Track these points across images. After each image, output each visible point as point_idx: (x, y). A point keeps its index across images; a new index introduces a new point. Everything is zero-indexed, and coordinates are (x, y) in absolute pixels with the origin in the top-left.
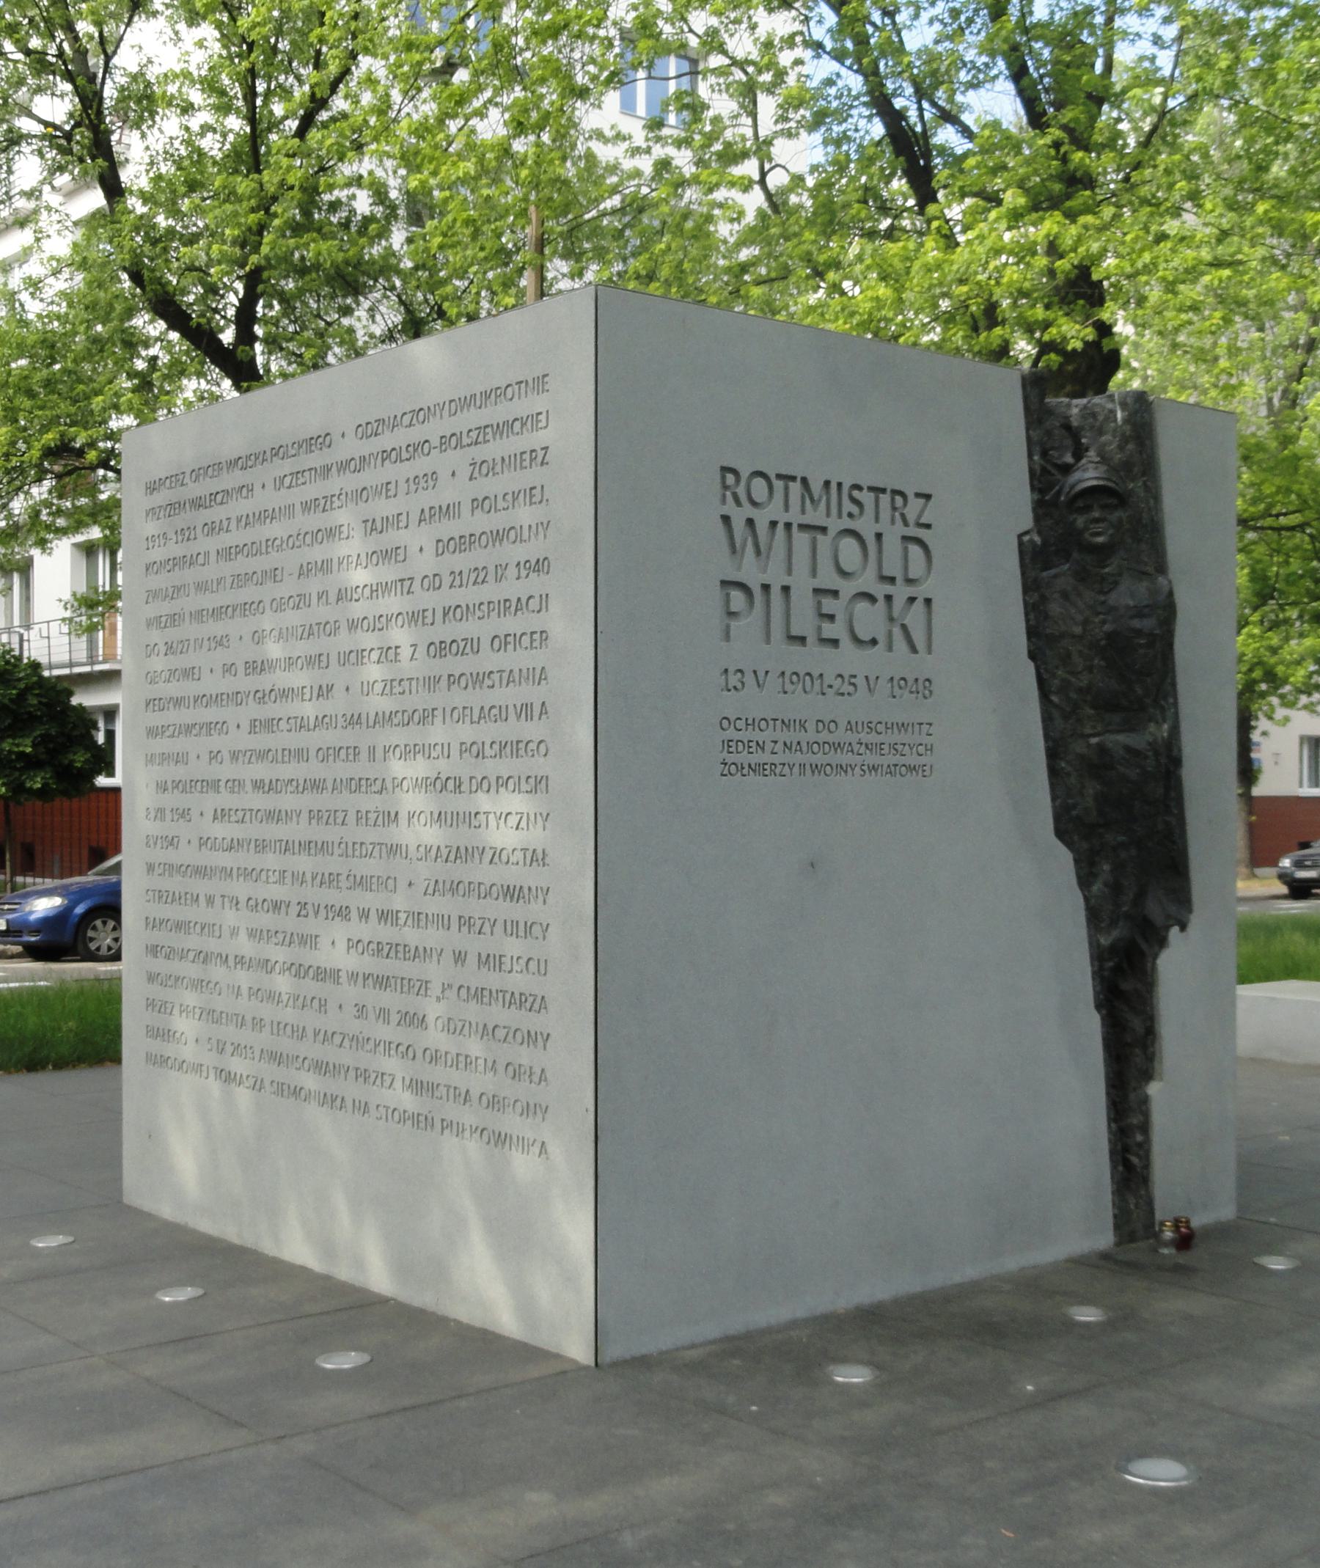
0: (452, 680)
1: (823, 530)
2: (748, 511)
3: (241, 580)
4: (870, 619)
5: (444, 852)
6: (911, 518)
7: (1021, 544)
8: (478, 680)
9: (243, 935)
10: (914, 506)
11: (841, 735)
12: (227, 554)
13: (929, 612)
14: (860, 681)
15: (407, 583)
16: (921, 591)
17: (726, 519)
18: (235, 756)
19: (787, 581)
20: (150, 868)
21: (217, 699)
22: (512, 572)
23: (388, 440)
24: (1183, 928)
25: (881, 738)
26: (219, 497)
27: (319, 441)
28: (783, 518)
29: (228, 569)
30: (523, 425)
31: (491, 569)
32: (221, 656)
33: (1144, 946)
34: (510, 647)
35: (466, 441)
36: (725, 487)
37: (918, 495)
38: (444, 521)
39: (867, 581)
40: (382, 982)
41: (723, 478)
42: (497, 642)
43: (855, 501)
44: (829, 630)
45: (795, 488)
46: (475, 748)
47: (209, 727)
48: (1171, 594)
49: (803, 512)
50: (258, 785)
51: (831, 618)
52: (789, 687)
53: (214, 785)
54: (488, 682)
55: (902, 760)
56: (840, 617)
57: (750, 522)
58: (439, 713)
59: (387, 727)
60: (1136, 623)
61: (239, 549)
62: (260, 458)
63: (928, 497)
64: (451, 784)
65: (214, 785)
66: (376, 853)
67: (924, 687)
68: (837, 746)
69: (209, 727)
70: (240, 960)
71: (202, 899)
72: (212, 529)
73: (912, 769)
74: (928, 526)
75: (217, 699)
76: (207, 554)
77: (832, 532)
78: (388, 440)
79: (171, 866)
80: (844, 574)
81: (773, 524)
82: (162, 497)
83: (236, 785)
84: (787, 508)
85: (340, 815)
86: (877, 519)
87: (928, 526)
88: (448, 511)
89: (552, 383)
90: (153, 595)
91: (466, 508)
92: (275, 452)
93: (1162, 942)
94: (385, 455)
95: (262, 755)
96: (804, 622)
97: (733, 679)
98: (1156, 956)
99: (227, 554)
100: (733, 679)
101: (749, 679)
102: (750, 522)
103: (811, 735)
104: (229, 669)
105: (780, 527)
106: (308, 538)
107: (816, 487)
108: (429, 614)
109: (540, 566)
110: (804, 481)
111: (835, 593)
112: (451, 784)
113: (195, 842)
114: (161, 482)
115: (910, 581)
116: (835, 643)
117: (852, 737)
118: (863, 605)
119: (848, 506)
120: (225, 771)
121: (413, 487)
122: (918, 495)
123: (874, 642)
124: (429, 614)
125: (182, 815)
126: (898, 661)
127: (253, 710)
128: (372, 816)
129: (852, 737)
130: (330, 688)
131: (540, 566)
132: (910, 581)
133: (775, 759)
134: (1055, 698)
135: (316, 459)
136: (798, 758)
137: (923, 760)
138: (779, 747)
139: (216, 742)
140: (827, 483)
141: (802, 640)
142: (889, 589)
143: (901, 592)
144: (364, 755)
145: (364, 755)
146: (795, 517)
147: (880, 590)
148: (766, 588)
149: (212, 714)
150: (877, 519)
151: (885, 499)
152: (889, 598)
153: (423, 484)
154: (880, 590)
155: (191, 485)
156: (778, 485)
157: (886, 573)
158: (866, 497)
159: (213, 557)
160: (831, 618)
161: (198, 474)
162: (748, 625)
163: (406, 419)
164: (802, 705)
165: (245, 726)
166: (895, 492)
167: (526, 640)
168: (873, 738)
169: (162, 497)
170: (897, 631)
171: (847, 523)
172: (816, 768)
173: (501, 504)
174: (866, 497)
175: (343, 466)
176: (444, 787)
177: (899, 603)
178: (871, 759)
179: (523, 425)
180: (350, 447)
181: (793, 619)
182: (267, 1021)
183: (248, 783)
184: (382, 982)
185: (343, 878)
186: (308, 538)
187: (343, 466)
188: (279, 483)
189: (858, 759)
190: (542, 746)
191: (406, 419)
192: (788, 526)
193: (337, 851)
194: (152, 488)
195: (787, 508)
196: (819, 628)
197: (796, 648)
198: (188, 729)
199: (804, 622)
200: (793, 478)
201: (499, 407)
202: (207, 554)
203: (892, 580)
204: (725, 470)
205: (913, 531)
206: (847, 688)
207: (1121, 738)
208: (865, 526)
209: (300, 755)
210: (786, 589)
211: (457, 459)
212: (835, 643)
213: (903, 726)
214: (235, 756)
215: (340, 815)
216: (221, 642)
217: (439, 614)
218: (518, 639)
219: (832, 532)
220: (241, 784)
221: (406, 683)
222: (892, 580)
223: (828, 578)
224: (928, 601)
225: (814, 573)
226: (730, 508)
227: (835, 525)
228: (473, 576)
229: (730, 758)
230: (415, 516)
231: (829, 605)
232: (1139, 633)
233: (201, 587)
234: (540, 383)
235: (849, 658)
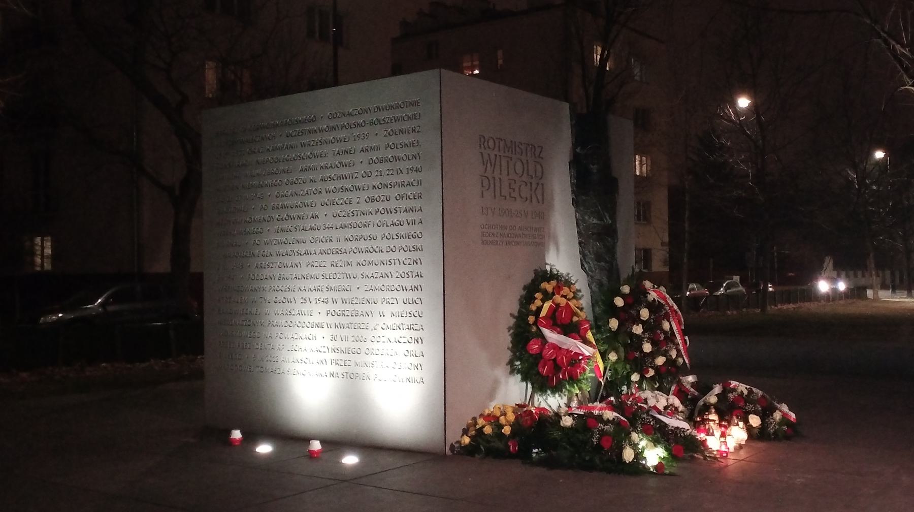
45: (502, 144)
156: (497, 142)
177: (534, 186)
184: (342, 326)
224: (543, 185)
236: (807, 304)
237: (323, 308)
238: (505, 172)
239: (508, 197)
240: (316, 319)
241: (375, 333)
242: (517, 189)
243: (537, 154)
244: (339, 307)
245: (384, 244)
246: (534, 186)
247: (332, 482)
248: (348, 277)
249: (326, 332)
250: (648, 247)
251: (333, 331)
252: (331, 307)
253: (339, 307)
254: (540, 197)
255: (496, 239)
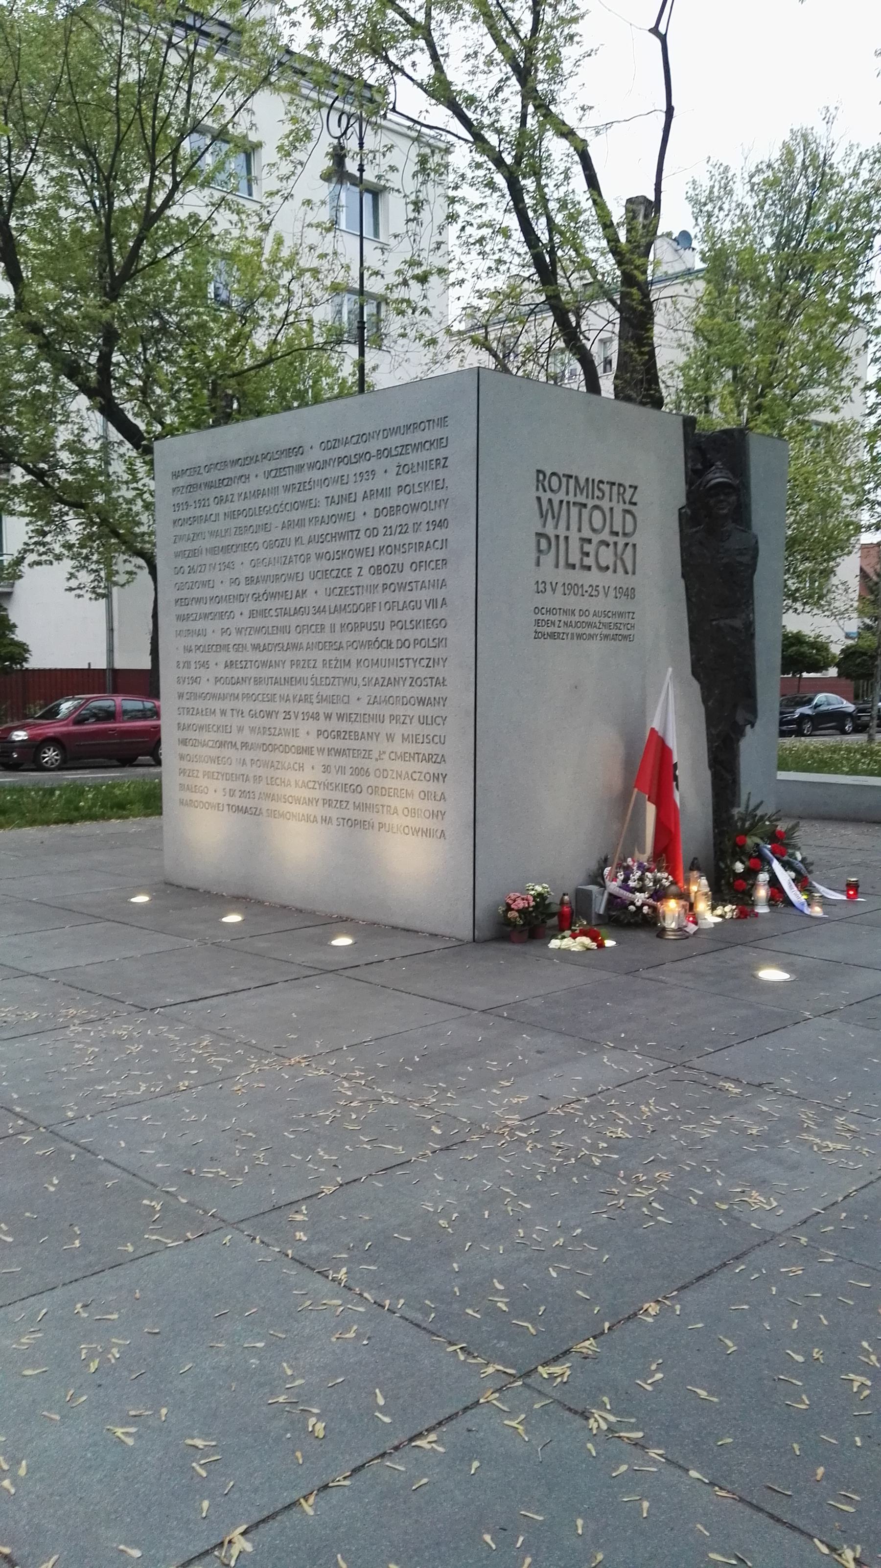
0: (385, 587)
1: (585, 506)
2: (549, 495)
3: (240, 530)
4: (606, 556)
5: (381, 681)
6: (627, 498)
7: (680, 514)
8: (402, 586)
9: (246, 731)
10: (629, 492)
11: (591, 619)
12: (232, 515)
13: (635, 552)
14: (600, 589)
15: (355, 533)
16: (632, 541)
17: (539, 499)
18: (239, 631)
19: (567, 533)
20: (181, 696)
21: (228, 599)
22: (424, 527)
23: (341, 452)
24: (753, 726)
25: (610, 620)
26: (225, 482)
27: (297, 450)
28: (566, 499)
29: (233, 524)
30: (432, 444)
31: (411, 525)
32: (228, 574)
33: (733, 736)
34: (423, 568)
35: (394, 453)
36: (538, 481)
37: (631, 486)
38: (380, 498)
39: (605, 536)
40: (339, 752)
41: (538, 476)
42: (414, 566)
43: (599, 489)
44: (587, 561)
45: (572, 482)
46: (400, 625)
47: (221, 615)
48: (757, 542)
49: (575, 495)
50: (256, 647)
51: (587, 554)
52: (567, 592)
53: (226, 648)
54: (408, 588)
55: (619, 632)
56: (592, 554)
57: (550, 501)
58: (377, 605)
59: (343, 613)
60: (739, 559)
61: (240, 512)
62: (252, 459)
63: (636, 488)
64: (385, 644)
65: (226, 648)
66: (336, 682)
67: (629, 593)
68: (589, 625)
69: (221, 615)
70: (245, 745)
71: (218, 711)
72: (220, 500)
73: (625, 637)
74: (635, 504)
75: (228, 599)
76: (218, 515)
77: (589, 506)
78: (341, 452)
79: (195, 694)
80: (594, 530)
81: (561, 502)
82: (182, 482)
83: (239, 648)
84: (567, 493)
85: (312, 663)
86: (611, 500)
87: (635, 504)
88: (384, 492)
89: (449, 421)
90: (177, 539)
91: (394, 491)
92: (264, 457)
93: (741, 733)
94: (341, 460)
95: (258, 630)
96: (574, 558)
97: (541, 588)
98: (738, 741)
99: (232, 515)
100: (541, 588)
101: (548, 587)
102: (550, 501)
103: (577, 618)
104: (235, 581)
105: (564, 503)
106: (288, 507)
107: (582, 482)
108: (370, 550)
109: (442, 524)
110: (576, 478)
111: (589, 541)
112: (385, 644)
113: (212, 680)
114: (184, 472)
115: (625, 534)
116: (589, 568)
117: (596, 620)
118: (603, 548)
119: (597, 493)
120: (235, 639)
121: (359, 479)
122: (631, 486)
123: (607, 568)
124: (370, 550)
125: (203, 666)
126: (616, 579)
127: (251, 605)
128: (334, 663)
129: (596, 620)
130: (304, 592)
131: (442, 524)
132: (625, 534)
133: (560, 630)
134: (694, 599)
135: (293, 461)
136: (570, 630)
137: (629, 632)
138: (562, 624)
139: (226, 623)
140: (587, 479)
141: (573, 567)
142: (615, 539)
143: (621, 540)
144: (327, 629)
145: (327, 629)
146: (571, 498)
147: (611, 539)
148: (557, 537)
149: (222, 607)
150: (611, 500)
151: (615, 488)
152: (616, 544)
153: (365, 476)
154: (611, 539)
155: (205, 474)
156: (564, 480)
157: (615, 529)
158: (606, 487)
159: (222, 516)
160: (587, 554)
161: (209, 468)
162: (548, 560)
163: (355, 440)
164: (573, 602)
165: (246, 613)
166: (620, 485)
167: (433, 565)
168: (606, 620)
169: (182, 482)
170: (619, 563)
171: (597, 502)
172: (579, 636)
173: (417, 489)
174: (606, 487)
175: (312, 466)
176: (380, 645)
177: (620, 547)
178: (606, 632)
179: (432, 444)
180: (316, 455)
181: (570, 555)
182: (264, 777)
183: (249, 646)
184: (339, 752)
185: (314, 697)
186: (288, 507)
187: (312, 466)
188: (267, 475)
189: (599, 631)
190: (443, 623)
191: (355, 440)
192: (568, 503)
193: (310, 682)
194: (176, 475)
195: (567, 493)
196: (582, 560)
197: (571, 571)
198: (206, 616)
199: (574, 558)
200: (571, 477)
201: (416, 434)
202: (218, 515)
203: (617, 534)
204: (539, 471)
205: (627, 507)
206: (594, 593)
207: (728, 621)
208: (605, 504)
209: (285, 630)
210: (567, 538)
211: (390, 463)
212: (589, 568)
213: (621, 614)
214: (239, 631)
215: (312, 663)
216: (229, 566)
217: (377, 550)
218: (428, 564)
219: (589, 506)
220: (244, 647)
221: (355, 589)
222: (617, 534)
223: (587, 533)
224: (634, 545)
225: (580, 530)
226: (541, 493)
227: (590, 503)
228: (398, 530)
229: (539, 629)
230: (360, 495)
231: (587, 548)
232: (741, 563)
233: (214, 534)
234: (442, 421)
235: (594, 577)
236: (672, 742)
237: (312, 726)
238: (574, 526)
239: (577, 566)
240: (301, 741)
241: (380, 765)
242: (592, 554)
243: (627, 498)
244: (335, 725)
245: (394, 635)
246: (620, 547)
247: (149, 132)
248: (347, 681)
249: (318, 760)
250: (166, 751)
251: (324, 759)
252: (323, 724)
253: (335, 725)
254: (630, 568)
255: (556, 630)
